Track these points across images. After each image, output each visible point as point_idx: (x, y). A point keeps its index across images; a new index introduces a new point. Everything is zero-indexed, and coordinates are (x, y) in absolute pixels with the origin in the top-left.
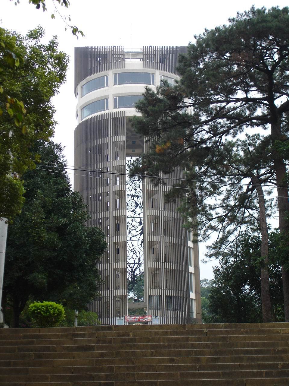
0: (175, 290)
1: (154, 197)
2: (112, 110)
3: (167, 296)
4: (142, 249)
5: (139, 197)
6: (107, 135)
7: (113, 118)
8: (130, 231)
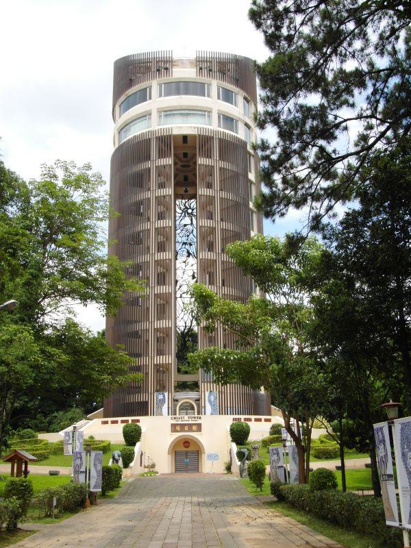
1: (208, 207)
6: (148, 158)
8: (180, 287)
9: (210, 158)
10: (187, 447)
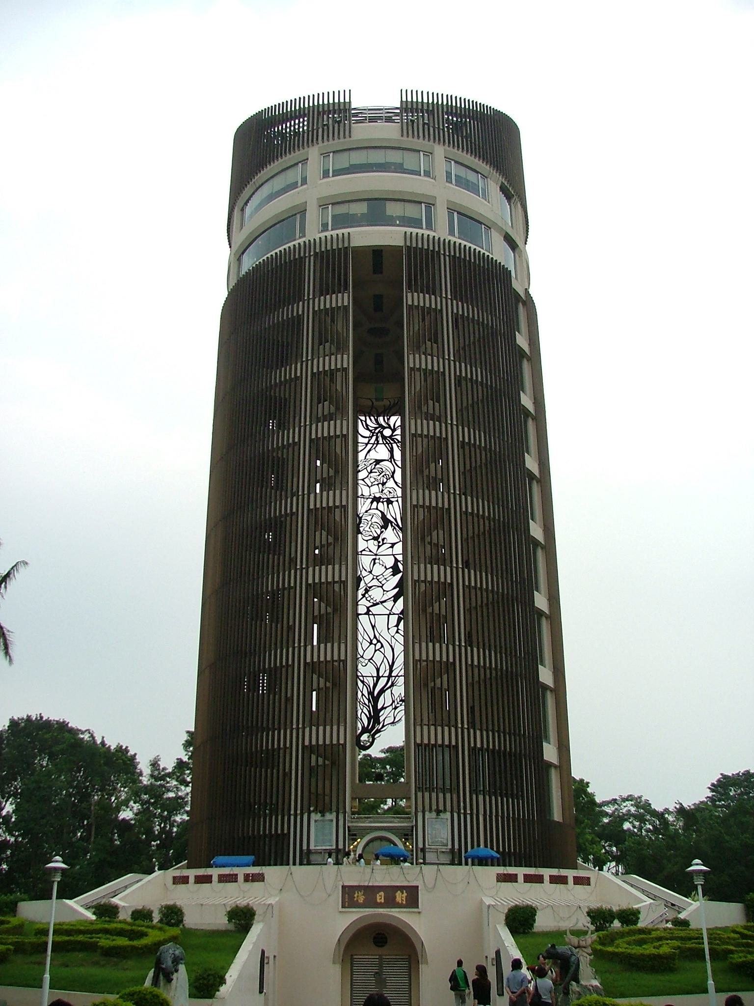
0: (498, 732)
1: (438, 681)
2: (313, 232)
3: (473, 750)
4: (401, 639)
5: (392, 502)
7: (316, 254)
8: (367, 591)
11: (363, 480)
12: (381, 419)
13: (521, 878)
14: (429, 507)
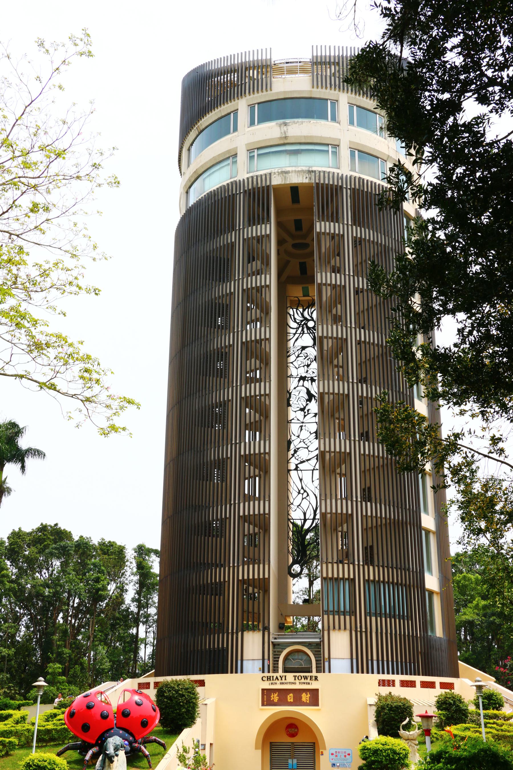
7: (245, 191)
9: (337, 221)
10: (293, 735)
11: (292, 363)
12: (306, 314)
13: (418, 684)
14: (333, 393)
